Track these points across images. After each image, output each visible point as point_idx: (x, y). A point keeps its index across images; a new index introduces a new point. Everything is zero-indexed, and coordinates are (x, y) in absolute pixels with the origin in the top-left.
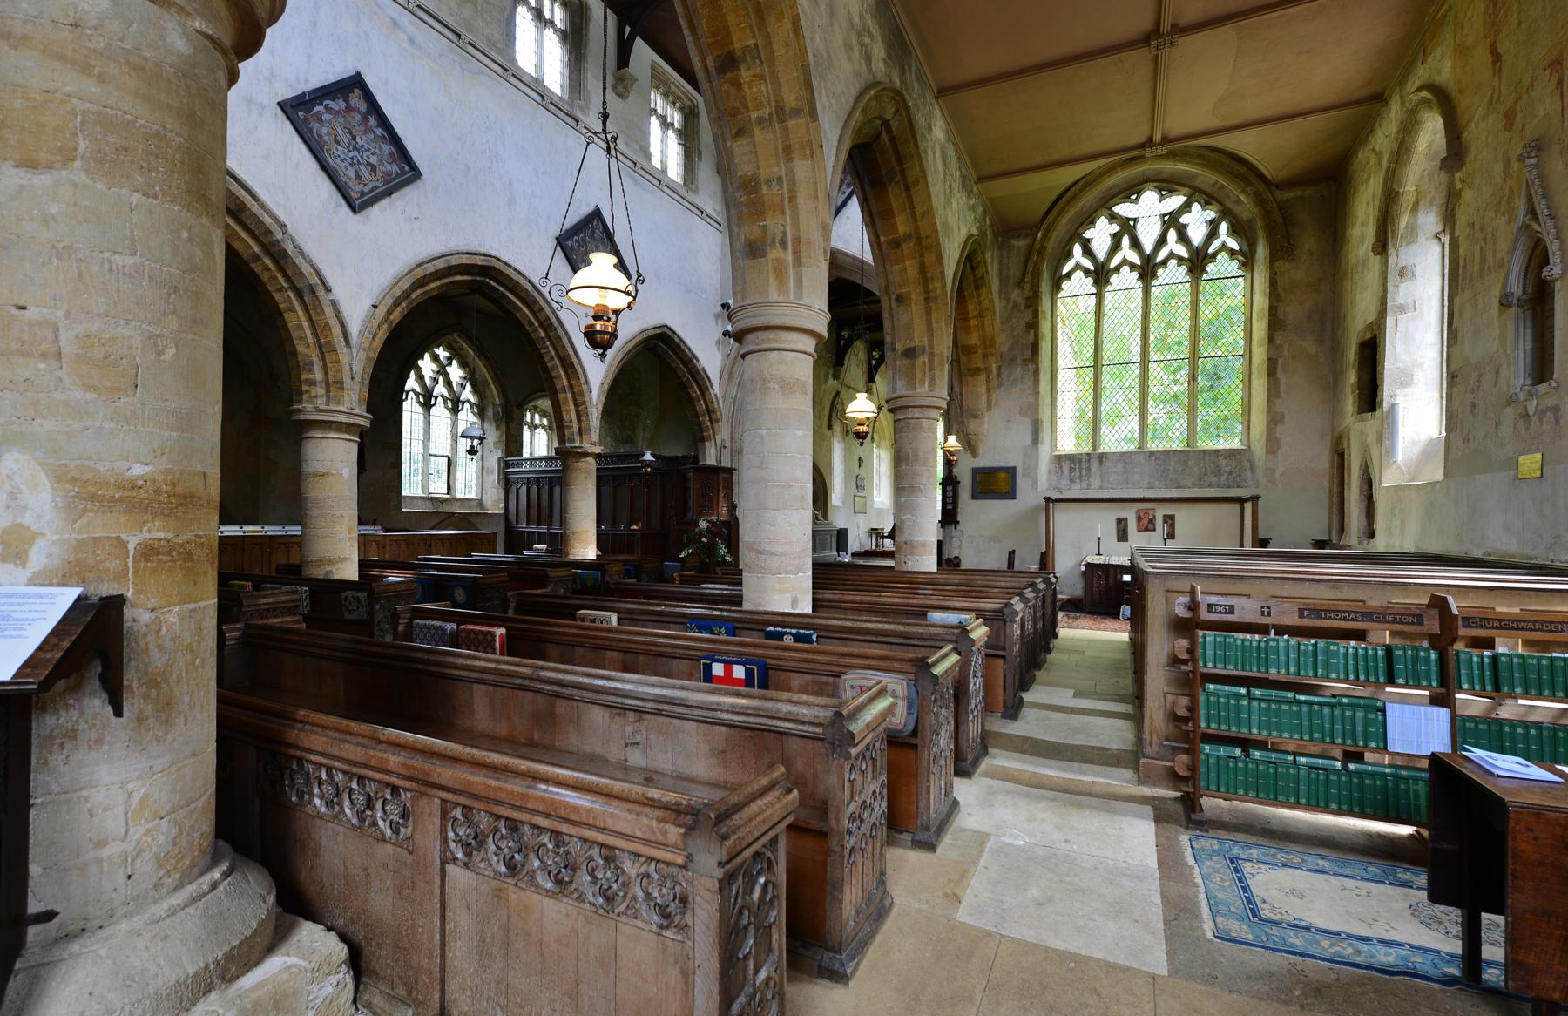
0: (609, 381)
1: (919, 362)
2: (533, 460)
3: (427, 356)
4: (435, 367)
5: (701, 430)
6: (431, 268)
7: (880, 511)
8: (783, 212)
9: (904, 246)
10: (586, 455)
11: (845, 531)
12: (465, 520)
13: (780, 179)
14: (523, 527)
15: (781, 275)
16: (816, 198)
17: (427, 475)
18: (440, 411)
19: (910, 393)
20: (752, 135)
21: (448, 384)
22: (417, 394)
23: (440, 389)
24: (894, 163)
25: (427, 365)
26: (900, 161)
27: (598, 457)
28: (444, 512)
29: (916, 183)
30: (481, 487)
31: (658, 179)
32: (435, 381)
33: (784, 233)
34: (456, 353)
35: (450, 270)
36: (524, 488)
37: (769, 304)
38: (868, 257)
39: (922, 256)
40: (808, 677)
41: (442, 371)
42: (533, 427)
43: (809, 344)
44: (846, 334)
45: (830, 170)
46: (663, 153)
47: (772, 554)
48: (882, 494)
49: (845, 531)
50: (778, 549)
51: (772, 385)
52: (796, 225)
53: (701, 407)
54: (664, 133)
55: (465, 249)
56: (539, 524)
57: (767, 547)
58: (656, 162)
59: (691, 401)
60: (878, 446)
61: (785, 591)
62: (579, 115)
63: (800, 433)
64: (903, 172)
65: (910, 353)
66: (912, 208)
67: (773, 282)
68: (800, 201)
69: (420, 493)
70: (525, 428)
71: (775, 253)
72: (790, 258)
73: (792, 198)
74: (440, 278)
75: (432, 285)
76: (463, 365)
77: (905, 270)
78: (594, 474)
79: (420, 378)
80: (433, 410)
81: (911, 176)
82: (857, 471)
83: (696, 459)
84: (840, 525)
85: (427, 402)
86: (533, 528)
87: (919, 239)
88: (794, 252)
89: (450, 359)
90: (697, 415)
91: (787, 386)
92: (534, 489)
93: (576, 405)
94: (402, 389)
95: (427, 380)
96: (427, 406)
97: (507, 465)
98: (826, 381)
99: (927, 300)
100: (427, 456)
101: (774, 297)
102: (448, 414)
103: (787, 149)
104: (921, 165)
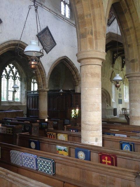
0: (51, 71)
1: (136, 63)
2: (34, 91)
3: (8, 66)
4: (10, 69)
5: (75, 83)
6: (4, 45)
7: (126, 103)
8: (91, 24)
9: (130, 30)
10: (45, 91)
11: (116, 109)
12: (17, 107)
13: (90, 15)
14: (31, 108)
15: (91, 43)
16: (101, 19)
17: (8, 95)
18: (11, 79)
19: (133, 73)
20: (81, 2)
21: (13, 73)
22: (5, 76)
23: (11, 74)
24: (126, 7)
25: (8, 69)
26: (128, 6)
27: (48, 91)
28: (12, 105)
29: (134, 12)
30: (21, 98)
31: (64, 18)
32: (10, 72)
33: (92, 30)
34: (15, 65)
35: (9, 45)
36: (31, 99)
37: (88, 51)
38: (119, 34)
39: (136, 33)
40: (98, 174)
41: (11, 70)
42: (34, 83)
43: (100, 62)
44: (115, 55)
45: (105, 10)
46: (65, 11)
47: (89, 125)
48: (126, 99)
49: (116, 109)
50: (91, 123)
51: (89, 75)
52: (95, 27)
53: (75, 77)
54: (65, 6)
55: (13, 40)
56: (35, 108)
57: (87, 123)
58: (63, 13)
59: (73, 76)
60: (125, 85)
61: (94, 136)
62: (42, 3)
63: (97, 89)
64: (129, 10)
65: (133, 61)
66: (132, 19)
67: (88, 45)
68: (97, 20)
69: (6, 100)
70: (32, 83)
71: (89, 36)
72: (94, 37)
73: (94, 20)
74: (7, 48)
75: (5, 49)
76: (16, 68)
77: (130, 37)
78: (47, 96)
79: (6, 72)
80: (9, 80)
81: (131, 10)
82: (119, 92)
83: (74, 91)
84: (114, 107)
85: (8, 77)
86: (33, 109)
87: (135, 28)
88: (95, 36)
89: (13, 67)
90: (74, 79)
91: (93, 75)
92: (34, 99)
93: (42, 78)
94: (2, 75)
95: (8, 72)
96: (8, 78)
97: (27, 93)
98: (110, 68)
99: (138, 45)
100: (8, 91)
101: (89, 49)
102: (13, 81)
103: (92, 6)
104: (135, 7)
